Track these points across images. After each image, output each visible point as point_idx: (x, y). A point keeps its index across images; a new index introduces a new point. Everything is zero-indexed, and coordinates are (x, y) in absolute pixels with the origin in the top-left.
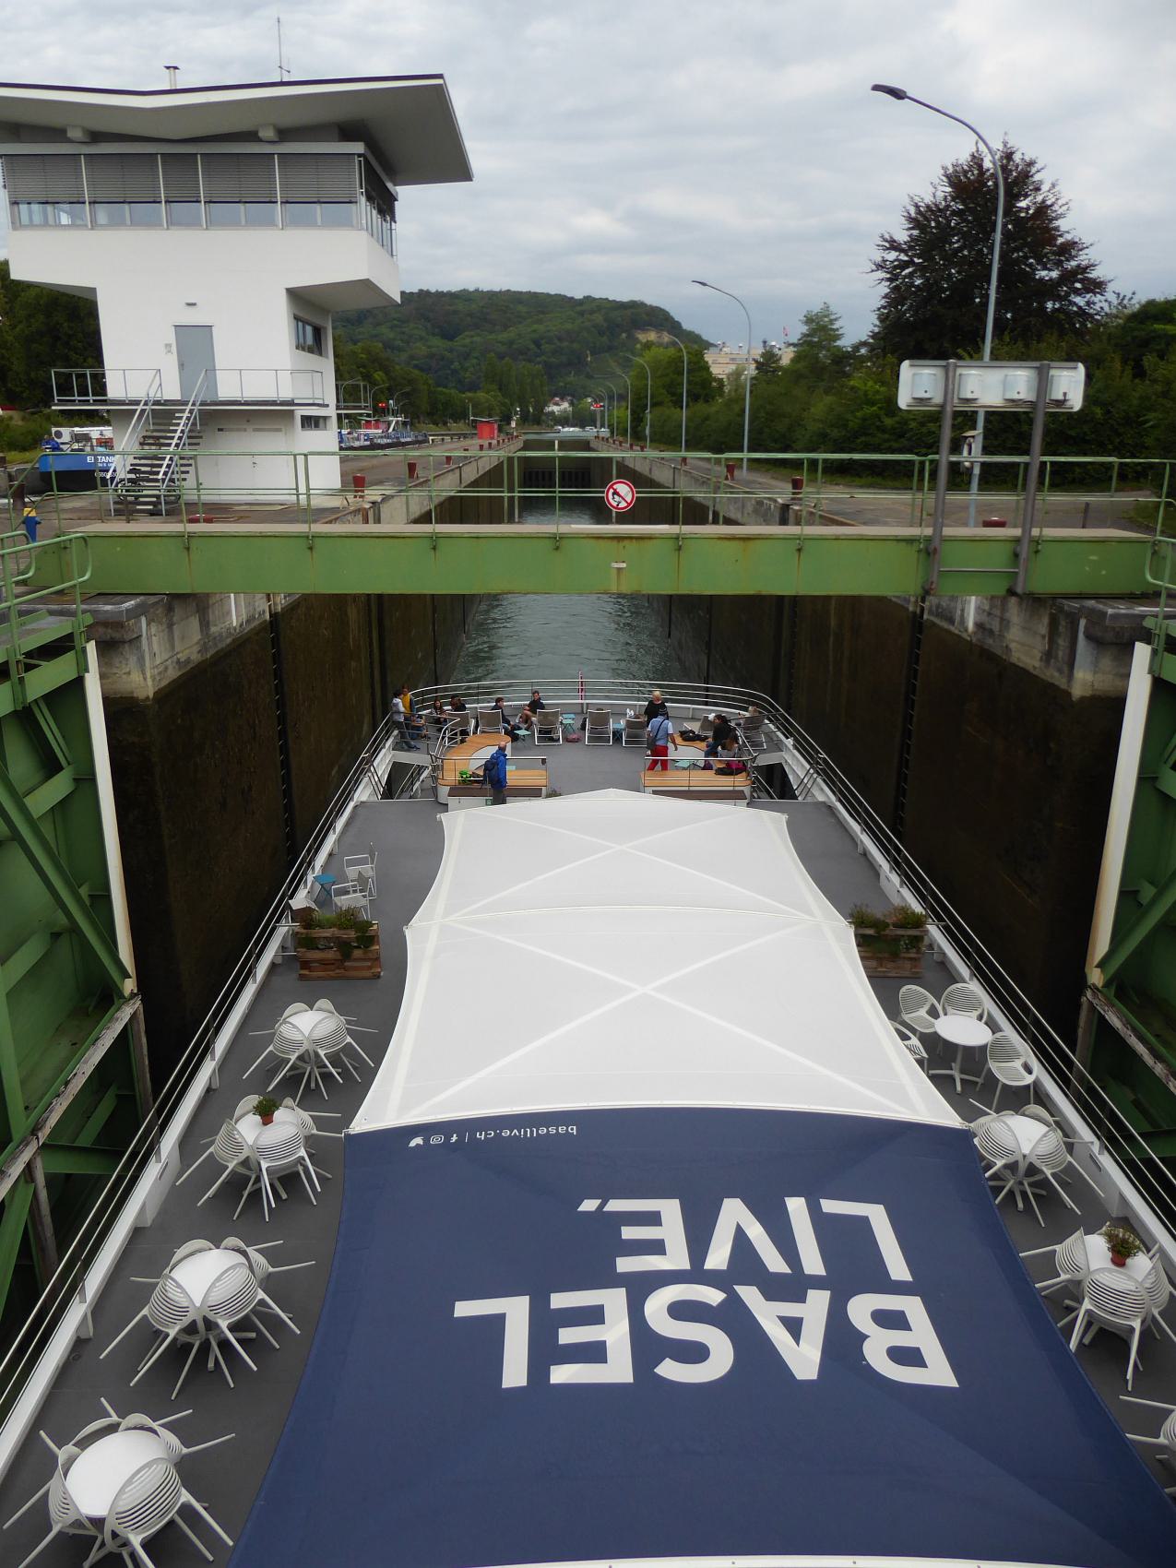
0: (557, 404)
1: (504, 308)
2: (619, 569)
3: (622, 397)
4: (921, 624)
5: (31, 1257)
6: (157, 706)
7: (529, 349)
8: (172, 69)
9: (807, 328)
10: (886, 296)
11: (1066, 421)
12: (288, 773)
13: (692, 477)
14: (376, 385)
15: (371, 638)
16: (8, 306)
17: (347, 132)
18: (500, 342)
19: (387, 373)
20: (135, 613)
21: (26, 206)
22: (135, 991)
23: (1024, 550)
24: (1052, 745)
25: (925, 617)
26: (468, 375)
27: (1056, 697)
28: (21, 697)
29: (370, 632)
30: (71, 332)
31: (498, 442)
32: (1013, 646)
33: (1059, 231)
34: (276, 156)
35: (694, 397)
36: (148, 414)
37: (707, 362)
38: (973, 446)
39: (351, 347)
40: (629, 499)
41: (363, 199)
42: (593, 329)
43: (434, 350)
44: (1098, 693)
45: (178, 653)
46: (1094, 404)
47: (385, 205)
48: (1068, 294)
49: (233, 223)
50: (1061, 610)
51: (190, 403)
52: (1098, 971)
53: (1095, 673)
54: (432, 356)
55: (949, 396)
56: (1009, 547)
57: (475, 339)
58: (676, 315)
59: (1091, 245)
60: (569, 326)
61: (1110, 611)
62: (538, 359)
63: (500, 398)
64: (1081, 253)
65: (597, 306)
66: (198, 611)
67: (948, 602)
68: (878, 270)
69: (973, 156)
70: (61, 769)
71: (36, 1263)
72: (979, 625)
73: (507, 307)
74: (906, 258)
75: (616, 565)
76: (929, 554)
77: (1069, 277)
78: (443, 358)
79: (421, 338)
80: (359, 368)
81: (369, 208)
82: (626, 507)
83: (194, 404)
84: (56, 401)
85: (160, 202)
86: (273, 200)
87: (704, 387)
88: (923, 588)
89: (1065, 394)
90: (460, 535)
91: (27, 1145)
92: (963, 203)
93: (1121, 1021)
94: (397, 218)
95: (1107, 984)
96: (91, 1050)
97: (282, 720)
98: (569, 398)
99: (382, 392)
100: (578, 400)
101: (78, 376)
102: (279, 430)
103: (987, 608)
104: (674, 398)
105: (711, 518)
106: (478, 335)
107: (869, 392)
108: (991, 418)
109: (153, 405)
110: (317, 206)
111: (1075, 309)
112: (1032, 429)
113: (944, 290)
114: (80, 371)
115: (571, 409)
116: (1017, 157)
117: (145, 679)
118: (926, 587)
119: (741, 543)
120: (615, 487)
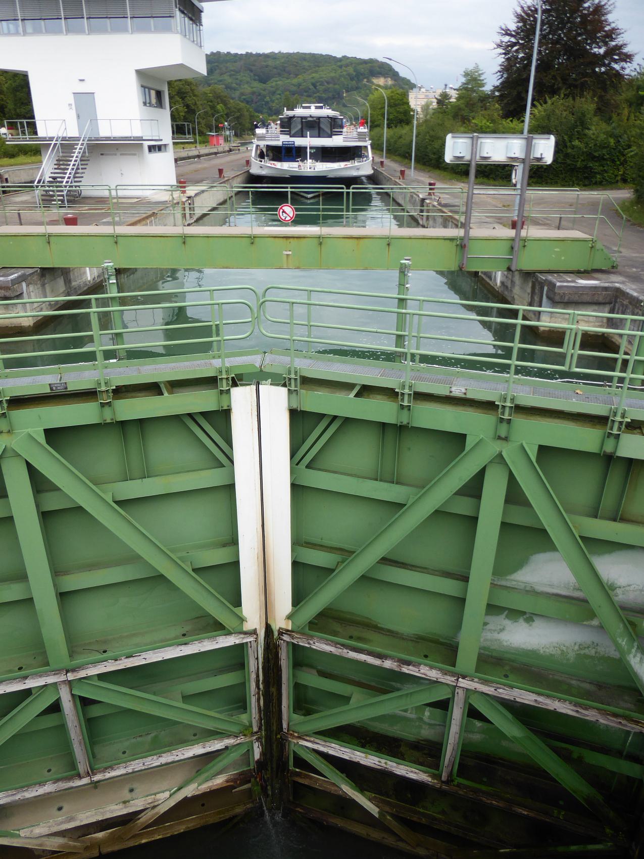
2: (287, 255)
7: (310, 89)
9: (465, 79)
14: (218, 113)
19: (225, 104)
20: (22, 278)
32: (516, 297)
33: (607, 22)
36: (58, 146)
38: (517, 171)
40: (291, 215)
41: (178, 13)
43: (254, 89)
49: (103, 31)
50: (537, 280)
51: (55, 139)
54: (253, 93)
55: (474, 155)
56: (508, 244)
57: (278, 82)
58: (396, 67)
60: (333, 74)
61: (558, 284)
62: (315, 95)
64: (618, 36)
65: (350, 62)
68: (498, 47)
72: (502, 283)
77: (611, 52)
78: (260, 95)
79: (248, 83)
80: (208, 102)
83: (83, 140)
86: (126, 16)
88: (459, 266)
89: (542, 154)
90: (198, 235)
92: (550, 5)
94: (203, 24)
101: (20, 122)
102: (135, 155)
106: (280, 80)
109: (61, 141)
110: (152, 20)
119: (356, 240)
120: (283, 208)
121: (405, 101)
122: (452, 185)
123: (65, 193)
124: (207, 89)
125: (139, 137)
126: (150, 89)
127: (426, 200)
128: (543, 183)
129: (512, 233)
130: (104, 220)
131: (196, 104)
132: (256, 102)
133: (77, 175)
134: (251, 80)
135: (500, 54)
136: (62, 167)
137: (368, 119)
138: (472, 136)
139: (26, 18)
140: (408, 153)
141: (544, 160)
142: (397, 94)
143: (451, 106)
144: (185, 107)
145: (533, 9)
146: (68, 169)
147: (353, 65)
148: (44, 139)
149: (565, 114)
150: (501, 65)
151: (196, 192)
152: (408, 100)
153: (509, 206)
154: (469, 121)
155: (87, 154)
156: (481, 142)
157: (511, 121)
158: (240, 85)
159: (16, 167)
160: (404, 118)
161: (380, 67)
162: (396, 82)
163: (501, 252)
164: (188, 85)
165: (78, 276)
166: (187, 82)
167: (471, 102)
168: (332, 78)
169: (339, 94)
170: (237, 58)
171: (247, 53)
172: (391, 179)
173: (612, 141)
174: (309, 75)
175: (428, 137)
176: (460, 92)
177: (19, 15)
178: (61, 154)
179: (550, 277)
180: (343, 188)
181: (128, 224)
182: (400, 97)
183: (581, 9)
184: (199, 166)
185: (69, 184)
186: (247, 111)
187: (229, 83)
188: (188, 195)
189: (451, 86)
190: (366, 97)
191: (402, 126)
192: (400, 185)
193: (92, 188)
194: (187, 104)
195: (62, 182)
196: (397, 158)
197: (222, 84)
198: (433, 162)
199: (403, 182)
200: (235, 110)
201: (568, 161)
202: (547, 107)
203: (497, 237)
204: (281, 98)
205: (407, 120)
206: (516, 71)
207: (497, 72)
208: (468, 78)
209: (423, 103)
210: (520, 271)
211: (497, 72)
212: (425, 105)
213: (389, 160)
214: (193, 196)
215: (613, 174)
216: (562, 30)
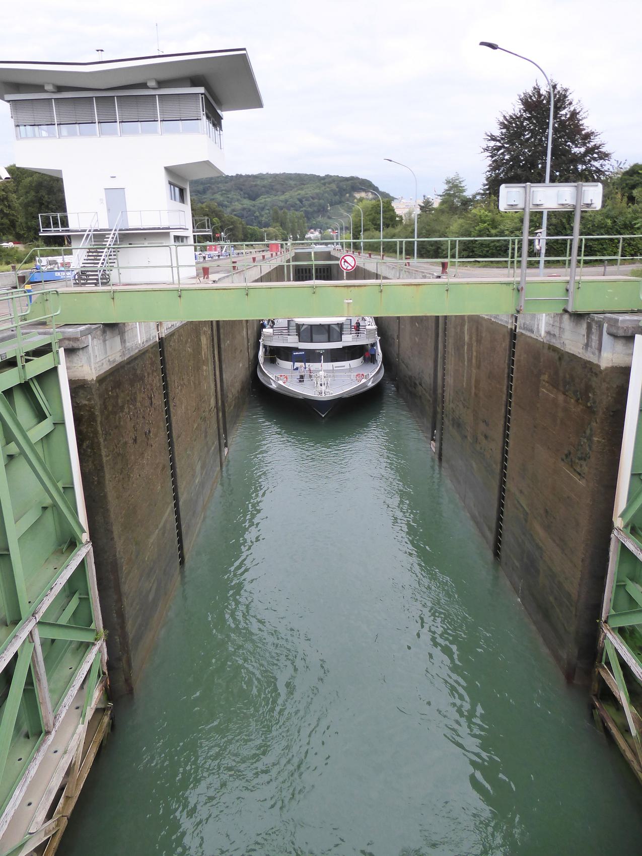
0: (312, 233)
3: (347, 228)
4: (515, 334)
6: (98, 384)
7: (296, 204)
8: (100, 51)
10: (490, 165)
11: (591, 228)
15: (214, 354)
16: (15, 188)
17: (195, 81)
18: (280, 201)
19: (220, 218)
20: (84, 334)
21: (24, 127)
23: (572, 288)
24: (590, 395)
25: (517, 330)
27: (590, 368)
28: (23, 376)
29: (214, 351)
30: (49, 200)
31: (281, 253)
32: (566, 342)
34: (157, 96)
35: (387, 226)
36: (91, 236)
37: (393, 207)
39: (200, 205)
40: (353, 265)
41: (205, 118)
44: (615, 365)
46: (606, 218)
47: (216, 121)
48: (590, 161)
50: (593, 320)
54: (244, 209)
56: (564, 286)
57: (267, 199)
58: (376, 183)
59: (602, 133)
60: (317, 191)
62: (301, 209)
63: (282, 231)
64: (596, 137)
65: (333, 180)
66: (119, 334)
67: (530, 321)
69: (535, 88)
70: (45, 417)
72: (548, 333)
74: (500, 145)
75: (346, 301)
76: (519, 290)
78: (250, 210)
79: (238, 200)
81: (208, 122)
82: (351, 269)
84: (42, 231)
85: (95, 123)
87: (392, 220)
89: (591, 200)
91: (29, 622)
95: (626, 527)
96: (65, 571)
97: (166, 396)
99: (218, 229)
103: (551, 322)
104: (376, 227)
107: (482, 216)
108: (550, 227)
110: (180, 122)
111: (594, 169)
112: (573, 232)
113: (522, 161)
114: (54, 214)
116: (559, 88)
117: (91, 369)
118: (518, 309)
119: (415, 286)
120: (345, 258)
132: (246, 218)
134: (241, 198)
135: (488, 157)
139: (62, 123)
147: (336, 182)
155: (118, 243)
158: (231, 202)
168: (317, 194)
169: (324, 208)
170: (228, 179)
171: (237, 175)
173: (609, 222)
174: (296, 191)
177: (56, 121)
178: (93, 243)
183: (559, 115)
198: (431, 252)
204: (269, 213)
208: (449, 185)
214: (217, 280)
215: (612, 251)
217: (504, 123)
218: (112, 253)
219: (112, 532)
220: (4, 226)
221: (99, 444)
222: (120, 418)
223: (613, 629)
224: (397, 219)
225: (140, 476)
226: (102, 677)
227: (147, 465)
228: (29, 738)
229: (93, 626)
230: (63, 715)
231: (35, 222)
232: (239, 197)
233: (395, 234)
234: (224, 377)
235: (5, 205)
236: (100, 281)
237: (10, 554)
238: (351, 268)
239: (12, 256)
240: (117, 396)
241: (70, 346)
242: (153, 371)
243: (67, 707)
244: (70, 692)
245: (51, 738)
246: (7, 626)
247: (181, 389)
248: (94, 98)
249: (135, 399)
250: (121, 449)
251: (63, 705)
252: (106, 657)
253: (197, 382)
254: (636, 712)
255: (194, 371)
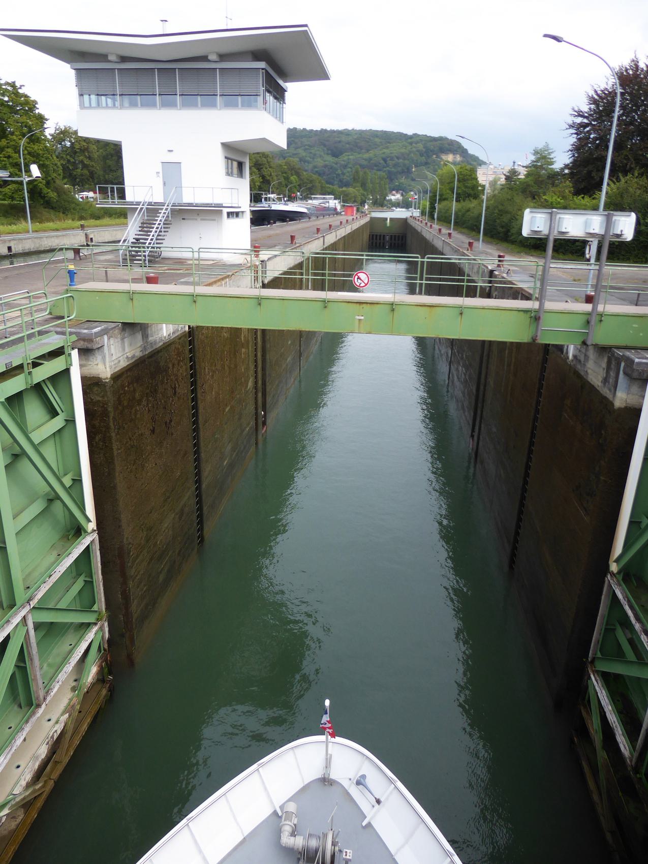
0: (394, 195)
1: (367, 140)
2: (360, 320)
5: (25, 662)
7: (380, 164)
12: (197, 412)
13: (451, 247)
14: (291, 183)
17: (257, 55)
20: (105, 332)
22: (96, 529)
23: (594, 320)
24: (603, 432)
26: (345, 177)
27: (607, 404)
32: (589, 371)
38: (591, 246)
42: (417, 153)
43: (326, 162)
45: (127, 353)
47: (279, 94)
50: (613, 355)
51: (166, 205)
52: (615, 564)
53: (628, 394)
54: (325, 166)
55: (552, 230)
56: (585, 318)
58: (465, 144)
60: (403, 150)
61: (637, 360)
62: (385, 169)
63: (362, 191)
65: (420, 139)
66: (141, 330)
68: (570, 128)
70: (58, 414)
71: (28, 667)
72: (575, 357)
73: (369, 139)
75: (358, 318)
78: (332, 168)
79: (321, 156)
80: (282, 173)
83: (168, 206)
86: (216, 94)
88: (532, 338)
89: (622, 231)
91: (23, 608)
93: (623, 596)
94: (286, 102)
95: (619, 572)
96: (66, 560)
98: (401, 192)
99: (295, 187)
100: (406, 193)
102: (214, 220)
105: (417, 291)
106: (352, 155)
115: (401, 198)
117: (106, 368)
119: (429, 308)
120: (358, 275)
121: (473, 176)
122: (520, 258)
123: (147, 253)
124: (281, 162)
125: (219, 204)
126: (232, 160)
127: (494, 272)
128: (615, 259)
129: (588, 307)
130: (182, 280)
131: (271, 175)
133: (159, 237)
134: (324, 154)
135: (572, 134)
136: (146, 229)
137: (436, 193)
138: (550, 212)
139: (124, 93)
140: (476, 225)
141: (624, 237)
142: (466, 169)
143: (520, 182)
144: (261, 178)
145: (606, 92)
146: (151, 232)
147: (423, 142)
148: (131, 203)
149: (638, 192)
150: (572, 145)
151: (270, 256)
152: (477, 176)
153: (579, 280)
154: (539, 196)
156: (560, 218)
157: (583, 198)
158: (313, 158)
159: (100, 228)
160: (472, 192)
161: (449, 145)
162: (465, 159)
163: (576, 326)
164: (265, 158)
165: (155, 332)
166: (264, 155)
167: (540, 179)
172: (459, 250)
174: (381, 150)
175: (496, 211)
176: (529, 169)
177: (157, 91)
178: (146, 218)
179: (628, 353)
180: (417, 258)
181: (206, 284)
182: (469, 173)
184: (272, 232)
185: (151, 245)
186: (319, 183)
187: (303, 156)
188: (261, 259)
189: (520, 163)
190: (434, 172)
191: (470, 201)
192: (468, 256)
193: (171, 249)
194: (263, 175)
195: (145, 243)
196: (465, 230)
197: (296, 158)
199: (471, 254)
200: (307, 181)
201: (641, 238)
202: (620, 185)
203: (573, 311)
204: (352, 171)
205: (475, 194)
206: (587, 151)
207: (568, 151)
209: (491, 179)
210: (596, 346)
211: (568, 151)
212: (493, 180)
213: (456, 232)
216: (636, 112)
217: (594, 98)
218: (163, 230)
219: (120, 521)
220: (83, 177)
221: (110, 438)
222: (136, 411)
223: (597, 672)
224: (480, 188)
225: (156, 464)
226: (103, 653)
227: (165, 453)
228: (21, 708)
229: (95, 608)
230: (55, 690)
231: (112, 175)
232: (322, 153)
233: (469, 208)
234: (268, 357)
235: (85, 156)
236: (147, 258)
237: (6, 547)
238: (364, 285)
239: (86, 210)
240: (134, 390)
241: (85, 347)
242: (179, 361)
243: (60, 683)
244: (65, 669)
245: (41, 711)
246: (3, 609)
247: (213, 375)
248: (156, 70)
249: (156, 391)
250: (135, 441)
251: (57, 680)
252: (107, 635)
253: (232, 366)
254: (606, 757)
255: (230, 355)
